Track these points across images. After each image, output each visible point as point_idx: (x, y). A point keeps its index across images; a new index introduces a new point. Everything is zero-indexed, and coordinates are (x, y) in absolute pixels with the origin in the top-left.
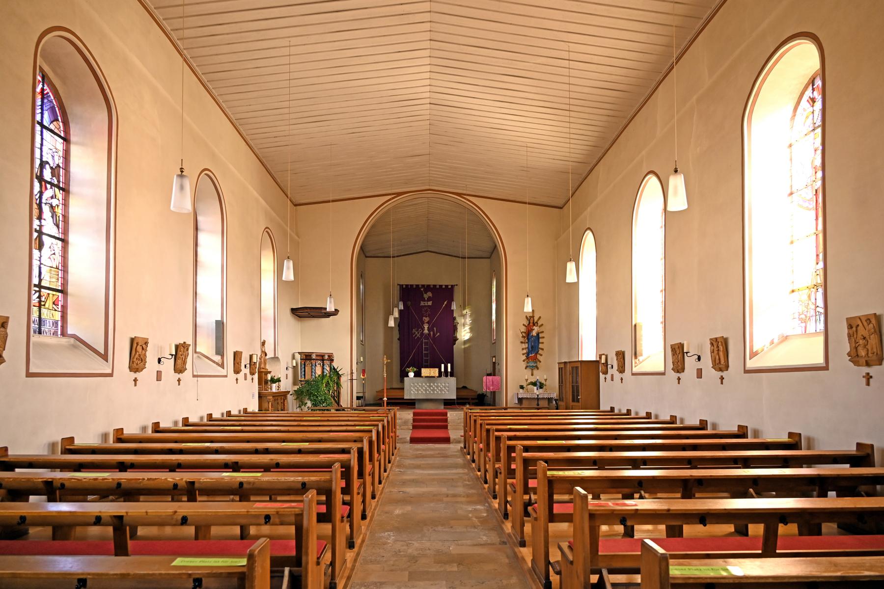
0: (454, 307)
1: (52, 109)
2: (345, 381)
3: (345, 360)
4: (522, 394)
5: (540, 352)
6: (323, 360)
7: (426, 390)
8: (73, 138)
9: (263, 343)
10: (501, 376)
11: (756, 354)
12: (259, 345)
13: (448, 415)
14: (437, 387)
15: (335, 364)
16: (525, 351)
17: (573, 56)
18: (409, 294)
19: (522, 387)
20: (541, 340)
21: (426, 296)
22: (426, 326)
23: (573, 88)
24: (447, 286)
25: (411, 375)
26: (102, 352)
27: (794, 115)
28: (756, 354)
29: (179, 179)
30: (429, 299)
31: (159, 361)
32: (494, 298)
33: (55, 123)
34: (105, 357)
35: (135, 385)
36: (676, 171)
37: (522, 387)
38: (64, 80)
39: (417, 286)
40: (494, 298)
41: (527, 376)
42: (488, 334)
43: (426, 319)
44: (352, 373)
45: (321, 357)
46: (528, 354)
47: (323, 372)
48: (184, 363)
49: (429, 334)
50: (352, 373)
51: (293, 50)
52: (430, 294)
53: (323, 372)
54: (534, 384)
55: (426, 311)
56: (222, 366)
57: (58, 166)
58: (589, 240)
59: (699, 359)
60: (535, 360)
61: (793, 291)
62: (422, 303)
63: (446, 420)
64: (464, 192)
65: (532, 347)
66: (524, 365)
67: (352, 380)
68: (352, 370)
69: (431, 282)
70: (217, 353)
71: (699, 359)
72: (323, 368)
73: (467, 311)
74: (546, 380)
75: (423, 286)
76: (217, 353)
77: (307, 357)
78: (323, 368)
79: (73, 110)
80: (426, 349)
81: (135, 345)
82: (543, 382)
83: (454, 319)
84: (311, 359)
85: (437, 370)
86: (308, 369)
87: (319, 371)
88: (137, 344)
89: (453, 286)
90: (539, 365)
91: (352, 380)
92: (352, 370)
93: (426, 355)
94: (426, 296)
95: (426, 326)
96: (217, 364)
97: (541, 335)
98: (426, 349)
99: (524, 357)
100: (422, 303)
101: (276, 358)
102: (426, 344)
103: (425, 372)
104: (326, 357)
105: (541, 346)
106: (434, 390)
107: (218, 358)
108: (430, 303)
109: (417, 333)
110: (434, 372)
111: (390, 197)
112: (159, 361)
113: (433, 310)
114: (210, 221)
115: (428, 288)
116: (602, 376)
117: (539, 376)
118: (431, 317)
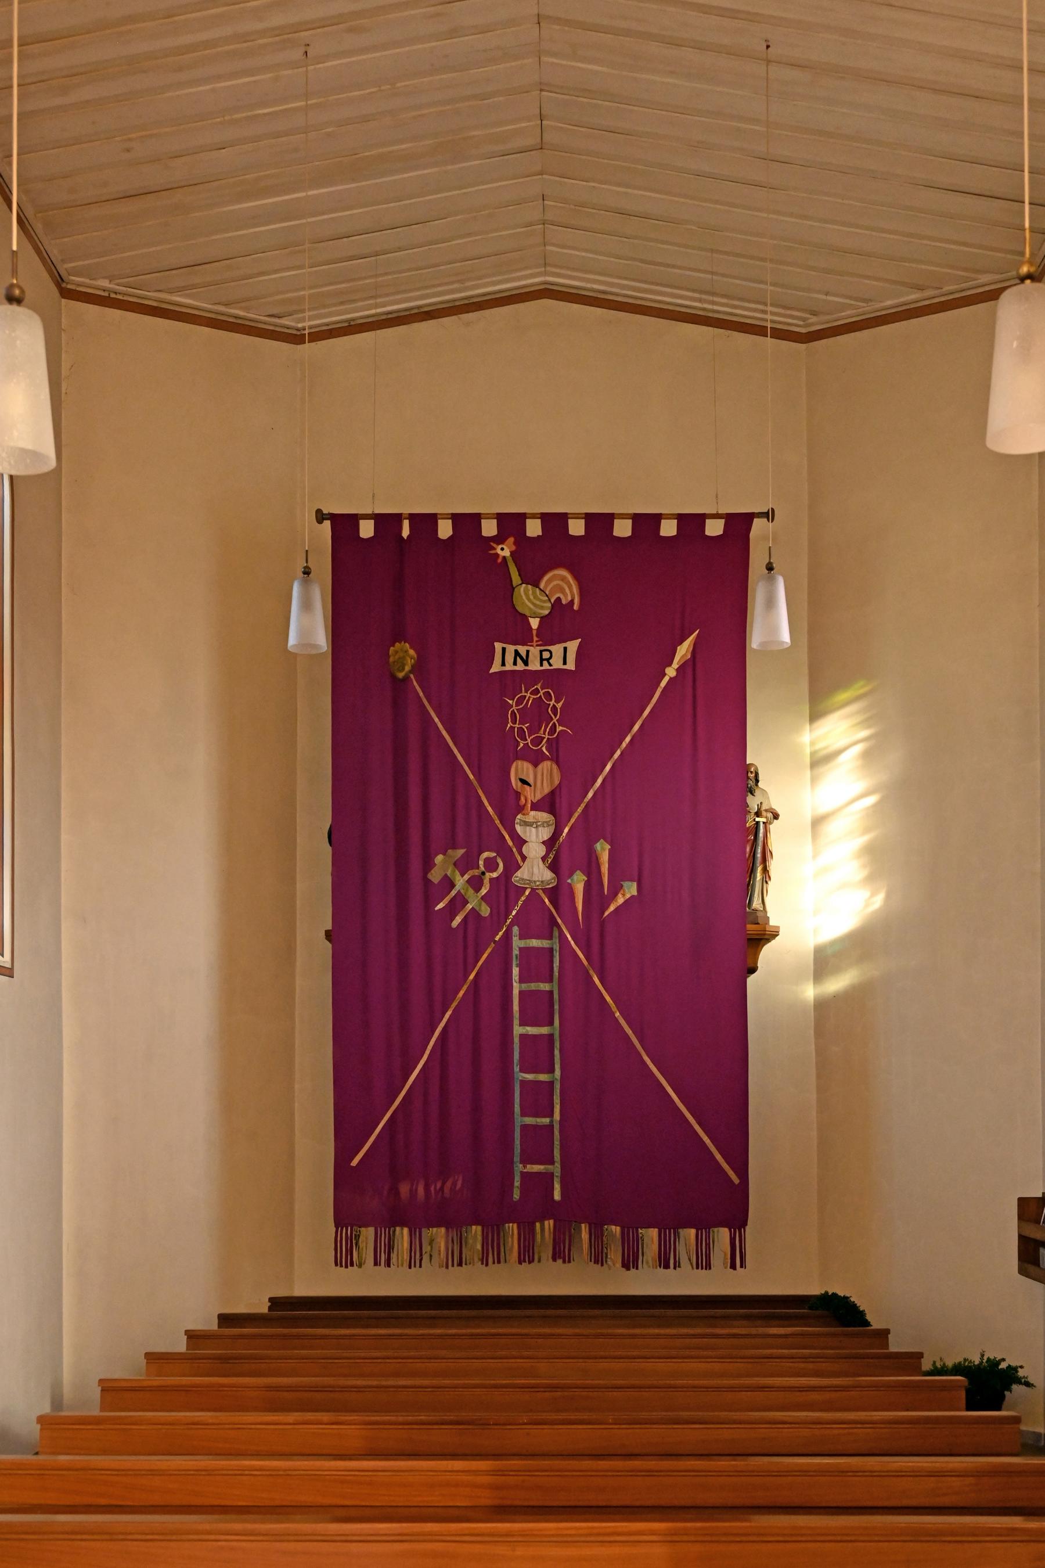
18: (406, 587)
21: (532, 602)
22: (535, 832)
30: (558, 624)
49: (558, 893)
52: (562, 585)
55: (538, 714)
62: (505, 658)
89: (739, 525)
93: (538, 1053)
95: (535, 832)
98: (537, 1008)
100: (505, 658)
102: (536, 965)
108: (565, 655)
113: (592, 701)
115: (552, 543)
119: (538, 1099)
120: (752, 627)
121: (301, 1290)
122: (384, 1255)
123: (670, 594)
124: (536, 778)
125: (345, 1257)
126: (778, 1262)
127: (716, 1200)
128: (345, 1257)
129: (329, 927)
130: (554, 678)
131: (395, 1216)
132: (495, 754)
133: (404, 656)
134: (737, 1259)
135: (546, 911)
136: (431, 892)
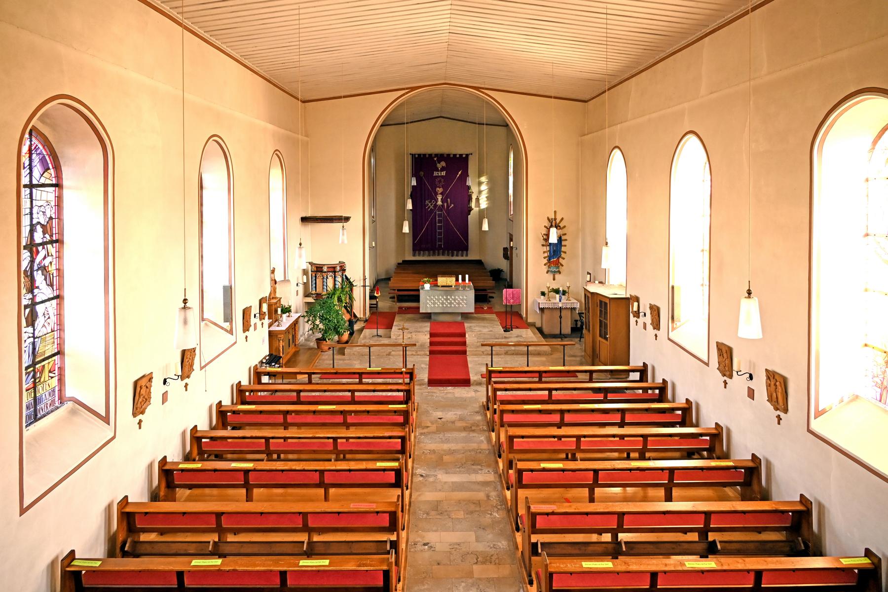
0: (470, 182)
1: (43, 161)
2: (358, 293)
3: (359, 271)
4: (542, 300)
5: (563, 255)
6: (335, 272)
7: (443, 303)
8: (65, 183)
9: (273, 272)
10: (519, 287)
11: (824, 412)
12: (268, 272)
13: (467, 336)
14: (454, 300)
15: (347, 273)
16: (546, 255)
17: (609, 12)
18: (423, 164)
19: (543, 294)
20: (563, 243)
21: (439, 166)
22: (440, 198)
23: (609, 31)
24: (461, 155)
25: (427, 286)
26: (104, 415)
27: (873, 148)
28: (824, 412)
29: (183, 312)
30: (443, 169)
31: (165, 382)
32: (511, 170)
33: (46, 174)
34: (106, 419)
35: (140, 428)
36: (749, 293)
37: (543, 294)
38: (53, 127)
39: (430, 155)
40: (511, 170)
41: (548, 282)
42: (507, 210)
43: (440, 190)
44: (365, 280)
45: (333, 269)
46: (550, 258)
47: (335, 284)
48: (191, 366)
49: (443, 206)
50: (365, 280)
51: (302, 11)
52: (443, 164)
53: (335, 284)
54: (557, 291)
55: (440, 181)
56: (231, 332)
57: (51, 218)
58: (617, 164)
59: (751, 377)
60: (558, 264)
61: (866, 345)
62: (435, 174)
63: (464, 344)
64: (483, 86)
65: (554, 251)
66: (545, 269)
67: (364, 286)
68: (364, 276)
69: (444, 149)
70: (226, 320)
71: (751, 377)
72: (335, 281)
73: (483, 179)
74: (569, 287)
75: (436, 155)
76: (226, 320)
77: (318, 269)
78: (335, 281)
79: (66, 154)
80: (440, 221)
81: (138, 389)
82: (566, 289)
83: (469, 188)
84: (322, 271)
85: (454, 279)
86: (319, 281)
87: (330, 283)
88: (141, 387)
89: (467, 155)
90: (561, 269)
91: (364, 286)
92: (364, 276)
93: (440, 228)
94: (439, 166)
95: (440, 198)
96: (226, 330)
97: (563, 238)
98: (440, 221)
99: (545, 261)
100: (435, 174)
101: (286, 281)
102: (440, 216)
103: (442, 280)
104: (338, 268)
105: (563, 249)
106: (451, 303)
107: (227, 325)
108: (444, 173)
109: (430, 205)
110: (451, 281)
111: (404, 92)
112: (165, 382)
113: (447, 180)
114: (215, 178)
115: (441, 157)
116: (633, 320)
117: (561, 282)
118: (445, 188)
119: (440, 234)
120: (45, 581)
121: (407, 259)
122: (419, 255)
123: (458, 164)
124: (440, 190)
125: (414, 255)
126: (472, 256)
127: (464, 247)
128: (414, 255)
129: (604, 249)
130: (442, 176)
131: (420, 250)
132: (434, 187)
133: (422, 173)
134: (467, 255)
135: (441, 208)
136: (426, 206)
